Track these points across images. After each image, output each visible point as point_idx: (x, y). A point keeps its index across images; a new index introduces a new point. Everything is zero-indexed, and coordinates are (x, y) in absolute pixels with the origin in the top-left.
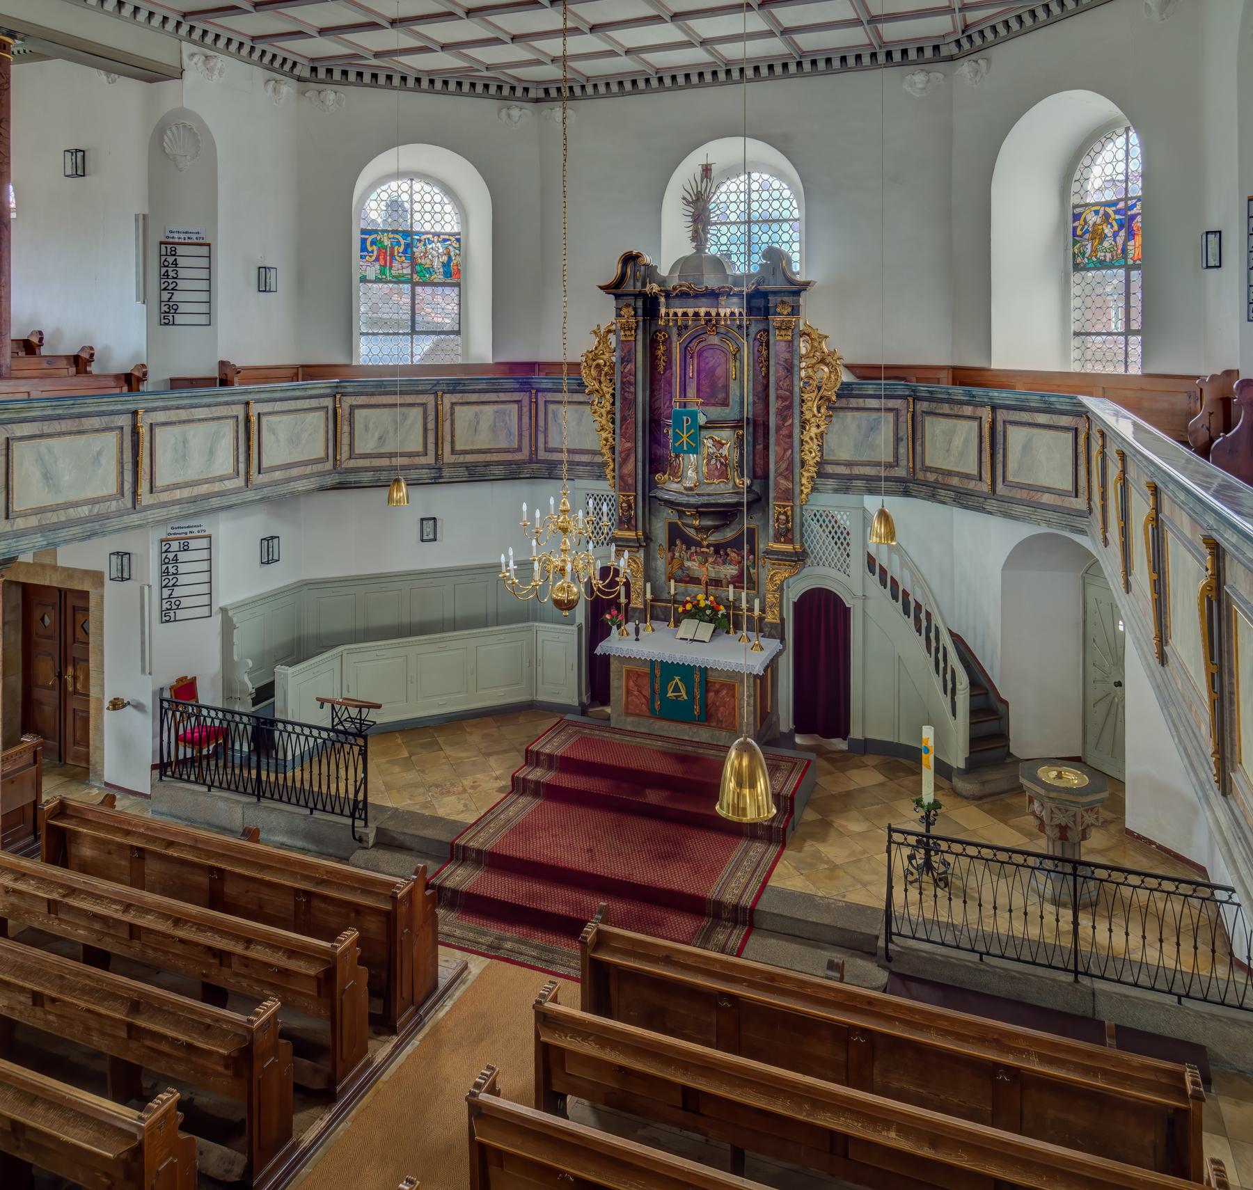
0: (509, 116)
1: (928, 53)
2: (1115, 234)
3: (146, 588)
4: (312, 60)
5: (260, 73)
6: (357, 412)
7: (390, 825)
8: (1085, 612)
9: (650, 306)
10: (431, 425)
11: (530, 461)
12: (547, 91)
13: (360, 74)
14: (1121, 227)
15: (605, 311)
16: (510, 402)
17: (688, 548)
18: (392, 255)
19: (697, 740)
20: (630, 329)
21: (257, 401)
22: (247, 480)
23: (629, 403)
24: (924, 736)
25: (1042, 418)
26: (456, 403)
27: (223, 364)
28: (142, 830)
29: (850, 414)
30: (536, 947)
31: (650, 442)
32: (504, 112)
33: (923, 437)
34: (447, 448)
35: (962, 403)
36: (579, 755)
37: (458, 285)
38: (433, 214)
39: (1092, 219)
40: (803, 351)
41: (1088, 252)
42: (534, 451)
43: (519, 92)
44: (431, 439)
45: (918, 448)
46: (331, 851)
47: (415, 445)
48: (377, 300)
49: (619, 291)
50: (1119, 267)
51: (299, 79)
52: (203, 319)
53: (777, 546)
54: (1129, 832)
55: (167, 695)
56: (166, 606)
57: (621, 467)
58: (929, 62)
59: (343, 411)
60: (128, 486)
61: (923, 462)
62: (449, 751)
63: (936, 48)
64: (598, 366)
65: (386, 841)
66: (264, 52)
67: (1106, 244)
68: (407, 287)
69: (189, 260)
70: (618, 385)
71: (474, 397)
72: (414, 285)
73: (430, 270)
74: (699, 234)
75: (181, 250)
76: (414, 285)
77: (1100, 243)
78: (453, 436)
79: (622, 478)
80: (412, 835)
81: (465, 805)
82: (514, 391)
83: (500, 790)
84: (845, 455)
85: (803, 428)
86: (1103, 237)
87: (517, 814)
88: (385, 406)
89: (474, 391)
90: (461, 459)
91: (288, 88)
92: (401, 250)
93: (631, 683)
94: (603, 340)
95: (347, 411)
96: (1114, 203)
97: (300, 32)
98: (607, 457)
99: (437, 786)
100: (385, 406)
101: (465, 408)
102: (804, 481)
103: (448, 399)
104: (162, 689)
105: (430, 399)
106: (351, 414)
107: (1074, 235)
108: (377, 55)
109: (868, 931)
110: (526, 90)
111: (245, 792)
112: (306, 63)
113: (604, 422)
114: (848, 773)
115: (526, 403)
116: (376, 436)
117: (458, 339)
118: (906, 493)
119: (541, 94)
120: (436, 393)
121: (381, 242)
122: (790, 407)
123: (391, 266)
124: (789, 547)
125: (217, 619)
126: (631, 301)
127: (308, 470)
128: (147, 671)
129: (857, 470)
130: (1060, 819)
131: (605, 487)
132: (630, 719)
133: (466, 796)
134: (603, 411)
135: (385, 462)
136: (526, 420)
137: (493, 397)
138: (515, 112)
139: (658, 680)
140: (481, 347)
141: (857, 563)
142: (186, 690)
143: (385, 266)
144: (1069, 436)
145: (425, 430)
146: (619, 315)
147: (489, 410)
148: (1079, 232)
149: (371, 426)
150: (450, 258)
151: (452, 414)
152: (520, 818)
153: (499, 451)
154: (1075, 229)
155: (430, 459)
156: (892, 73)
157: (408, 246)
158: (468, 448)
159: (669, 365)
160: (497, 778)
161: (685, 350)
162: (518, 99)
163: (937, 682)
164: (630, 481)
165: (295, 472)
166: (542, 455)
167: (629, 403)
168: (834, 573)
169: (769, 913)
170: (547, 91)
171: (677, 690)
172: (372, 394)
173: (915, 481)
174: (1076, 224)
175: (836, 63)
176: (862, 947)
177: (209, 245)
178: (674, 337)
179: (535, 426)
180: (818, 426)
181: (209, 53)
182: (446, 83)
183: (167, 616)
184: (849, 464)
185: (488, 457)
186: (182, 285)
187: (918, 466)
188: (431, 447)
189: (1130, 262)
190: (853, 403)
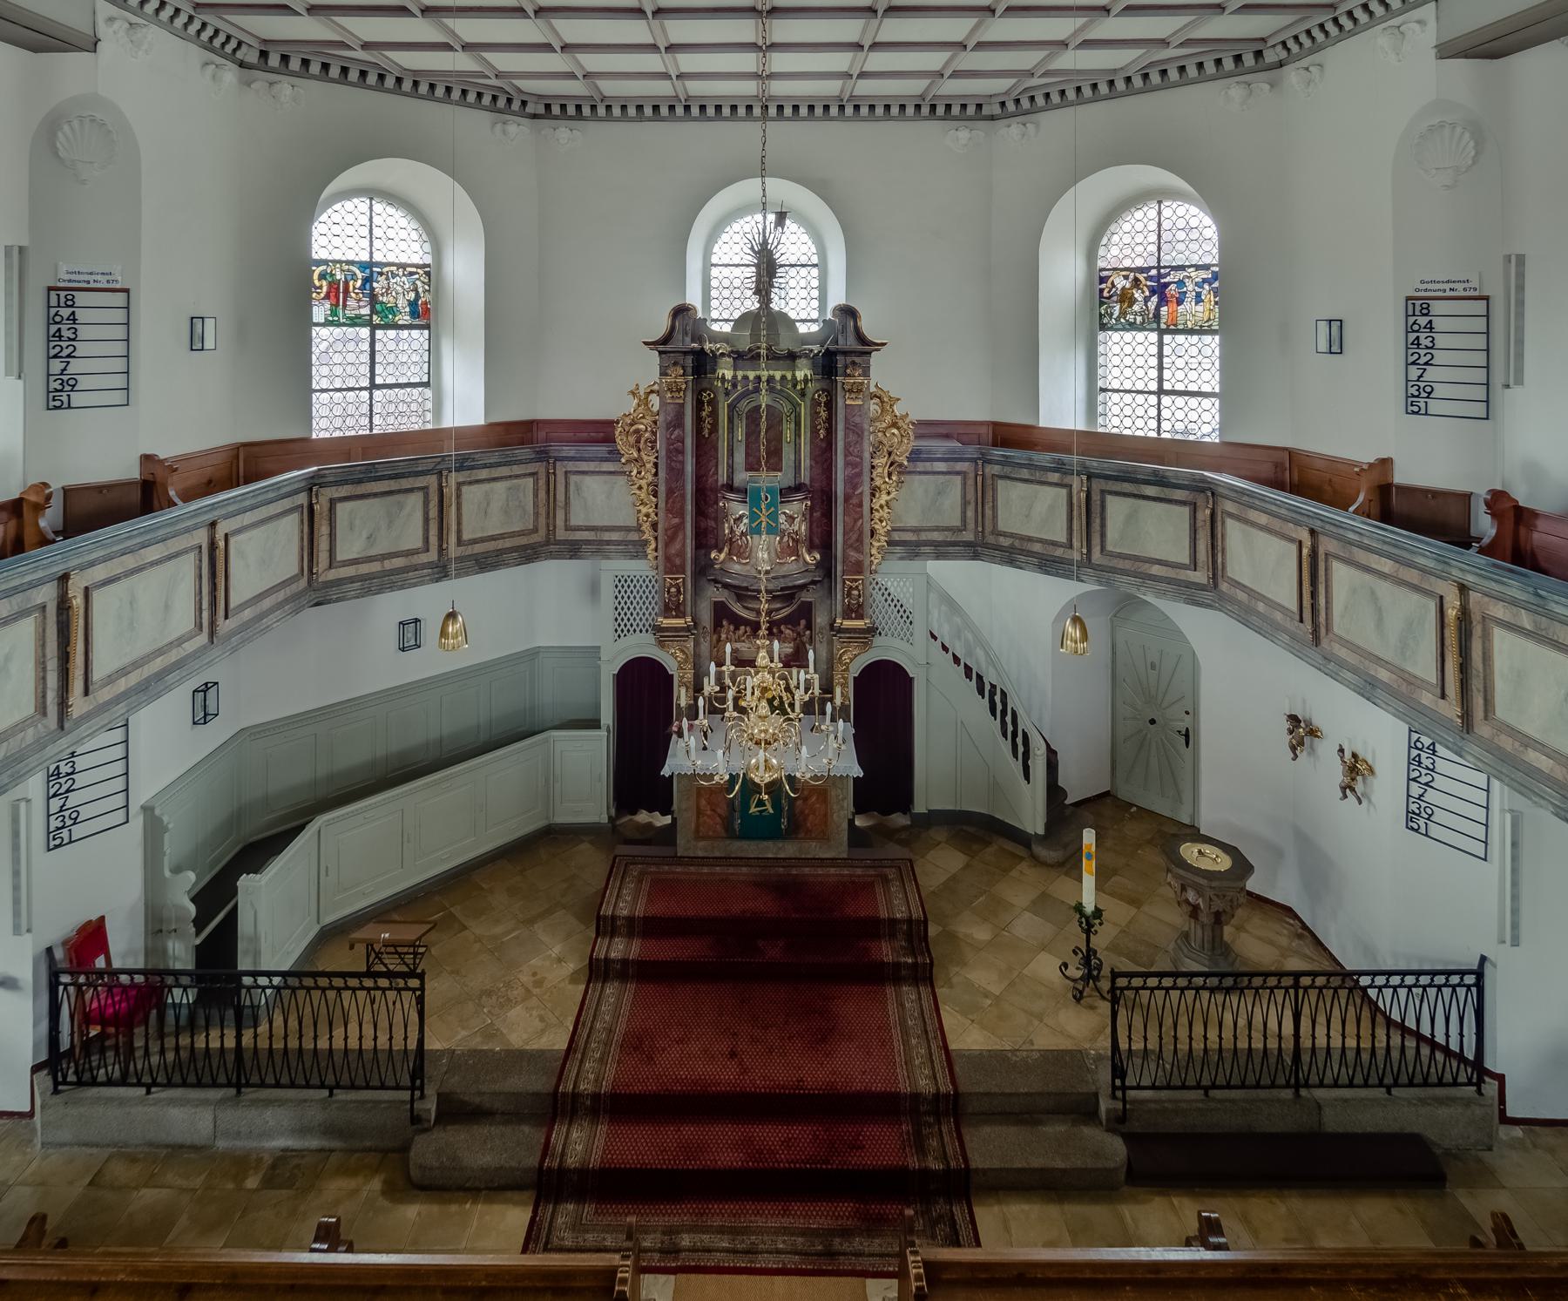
0: (504, 132)
1: (971, 110)
2: (1146, 300)
3: (23, 805)
4: (265, 41)
5: (196, 53)
6: (339, 506)
7: (454, 1083)
8: (1114, 653)
9: (702, 364)
10: (433, 513)
11: (547, 543)
12: (548, 107)
13: (325, 66)
14: (1153, 292)
16: (525, 475)
17: (737, 628)
18: (346, 291)
19: (782, 855)
20: (679, 390)
21: (226, 517)
22: (212, 634)
23: (676, 473)
24: (1085, 841)
25: (1150, 491)
26: (464, 483)
27: (147, 459)
28: (120, 1277)
29: (917, 477)
30: (721, 1230)
31: (697, 518)
32: (499, 126)
33: (994, 500)
34: (453, 539)
35: (1021, 466)
36: (661, 908)
37: (427, 327)
38: (400, 242)
39: (1120, 283)
41: (1116, 314)
42: (551, 529)
43: (516, 106)
44: (433, 532)
45: (988, 512)
46: (368, 1144)
48: (335, 351)
49: (668, 348)
50: (1152, 330)
51: (242, 64)
52: (118, 397)
53: (848, 624)
54: (1250, 894)
55: (59, 954)
56: (54, 824)
57: (667, 545)
58: (970, 119)
59: (321, 507)
60: (51, 696)
61: (995, 524)
62: (478, 928)
63: (979, 106)
64: (637, 431)
65: (455, 1112)
66: (204, 25)
67: (1136, 308)
68: (365, 332)
69: (94, 315)
70: (663, 453)
71: (484, 474)
72: (374, 328)
73: (393, 310)
74: (763, 288)
75: (81, 298)
76: (374, 328)
77: (1130, 306)
78: (459, 524)
79: (668, 558)
80: (494, 1094)
81: (542, 1019)
82: (531, 461)
83: (573, 979)
84: (912, 522)
85: (873, 495)
86: (1132, 301)
87: (616, 1016)
88: (375, 495)
89: (485, 466)
90: (469, 550)
91: (230, 74)
92: (359, 283)
93: (703, 802)
94: (645, 402)
95: (326, 506)
96: (1141, 270)
97: (285, 7)
98: (648, 535)
99: (489, 993)
101: (474, 488)
102: (874, 551)
103: (454, 478)
104: (49, 950)
105: (432, 480)
106: (332, 509)
107: (1101, 296)
108: (366, 46)
109: (1085, 1090)
110: (524, 103)
111: (214, 1084)
112: (255, 44)
113: (643, 495)
114: (929, 857)
115: (542, 476)
116: (365, 535)
117: (428, 393)
118: (976, 556)
119: (541, 110)
120: (440, 473)
121: (332, 275)
122: (860, 474)
123: (345, 306)
124: (859, 624)
125: (137, 822)
126: (680, 358)
127: (281, 596)
128: (24, 927)
129: (924, 536)
130: (1218, 905)
131: (641, 569)
132: (701, 844)
133: (534, 1001)
134: (643, 483)
135: (375, 567)
136: (542, 494)
137: (504, 471)
138: (512, 129)
140: (465, 404)
141: (920, 634)
142: (92, 937)
143: (337, 304)
144: (1186, 510)
145: (426, 520)
146: (663, 374)
147: (500, 487)
148: (1105, 294)
149: (357, 522)
150: (418, 296)
151: (459, 496)
152: (621, 1028)
153: (512, 535)
154: (1101, 291)
155: (432, 556)
156: (934, 127)
157: (368, 280)
158: (479, 535)
159: (714, 428)
160: (559, 960)
161: (732, 407)
162: (514, 114)
163: (1006, 746)
164: (678, 561)
165: (267, 603)
166: (561, 534)
167: (676, 473)
168: (897, 643)
169: (976, 1094)
170: (548, 107)
172: (360, 481)
173: (986, 546)
175: (880, 111)
176: (1082, 1110)
177: (127, 291)
178: (721, 397)
179: (550, 501)
181: (134, 19)
182: (432, 87)
183: (55, 840)
184: (916, 530)
185: (500, 544)
186: (82, 348)
187: (989, 528)
188: (433, 540)
189: (1163, 326)
190: (921, 466)
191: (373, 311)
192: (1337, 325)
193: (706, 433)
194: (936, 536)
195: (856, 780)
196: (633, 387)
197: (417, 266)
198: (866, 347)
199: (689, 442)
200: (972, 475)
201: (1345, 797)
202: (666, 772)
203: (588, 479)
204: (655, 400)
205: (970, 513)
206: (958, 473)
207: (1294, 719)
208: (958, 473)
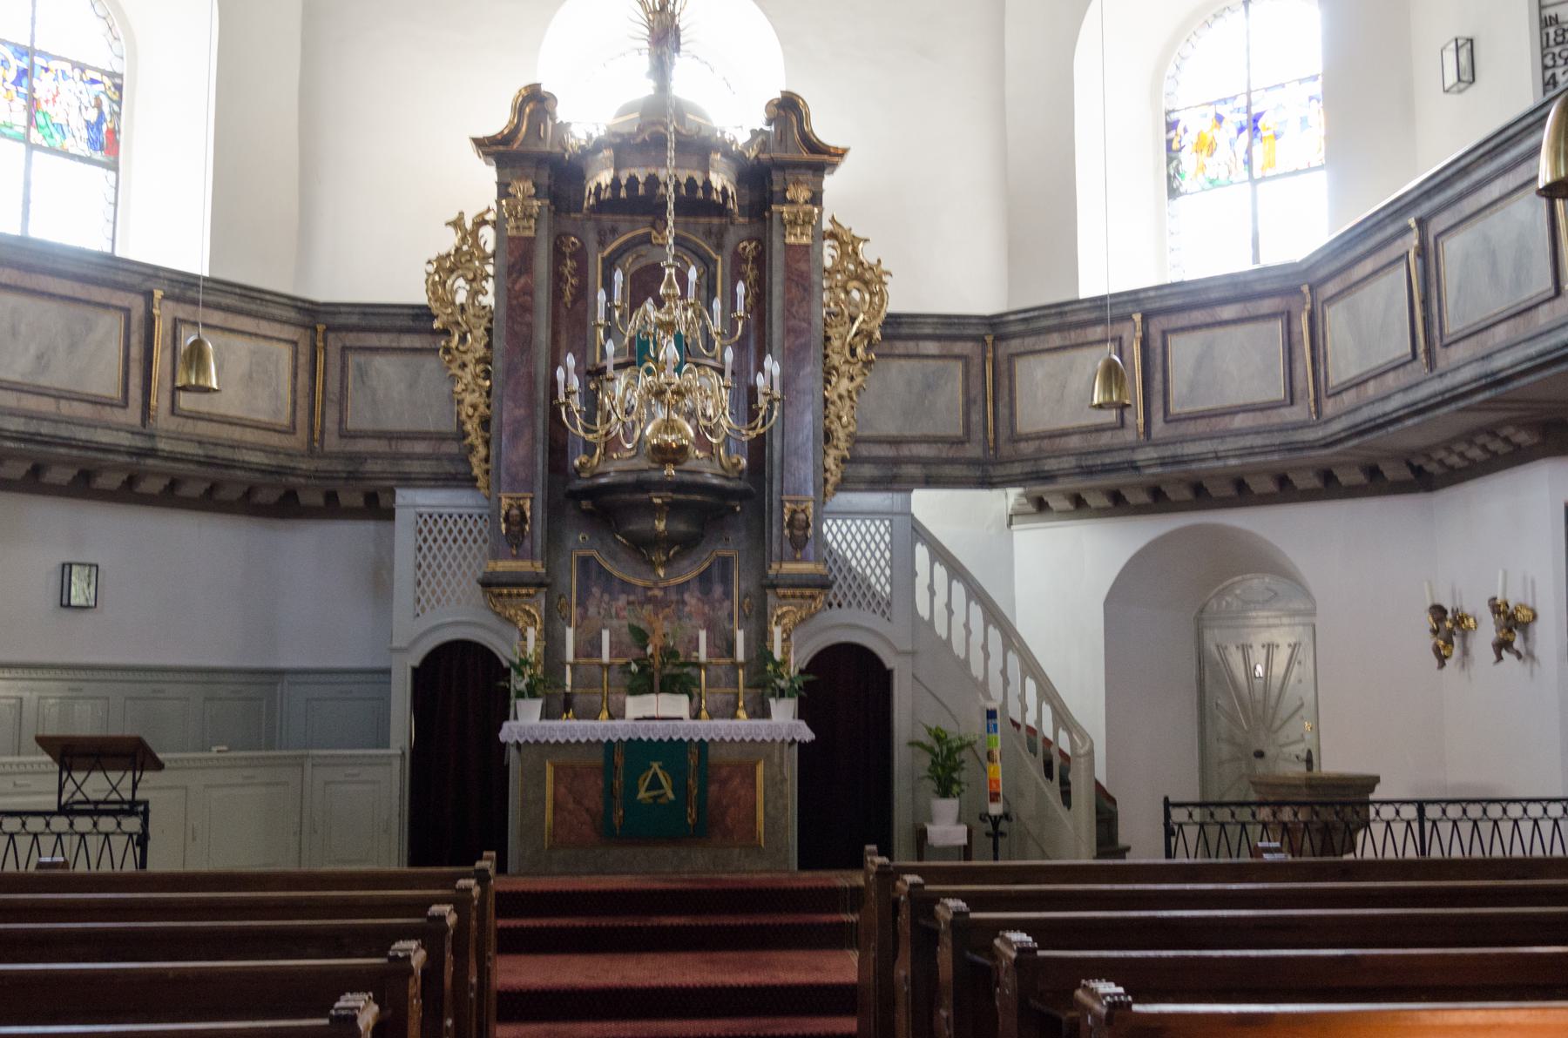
15: (479, 186)
16: (279, 340)
26: (184, 321)
33: (1012, 390)
40: (828, 263)
47: (105, 381)
84: (890, 428)
88: (52, 296)
90: (189, 427)
93: (562, 790)
100: (52, 296)
116: (33, 350)
129: (905, 451)
139: (621, 771)
149: (23, 328)
150: (101, 114)
155: (133, 416)
171: (656, 786)
174: (1172, 134)
180: (852, 379)
190: (900, 347)
191: (31, 120)
192: (1468, 47)
193: (568, 297)
194: (923, 450)
195: (802, 746)
196: (453, 216)
197: (104, 73)
198: (821, 159)
199: (543, 298)
200: (977, 361)
201: (1500, 658)
202: (504, 735)
203: (379, 361)
204: (488, 236)
205: (976, 417)
206: (957, 357)
207: (1438, 612)
208: (957, 357)
